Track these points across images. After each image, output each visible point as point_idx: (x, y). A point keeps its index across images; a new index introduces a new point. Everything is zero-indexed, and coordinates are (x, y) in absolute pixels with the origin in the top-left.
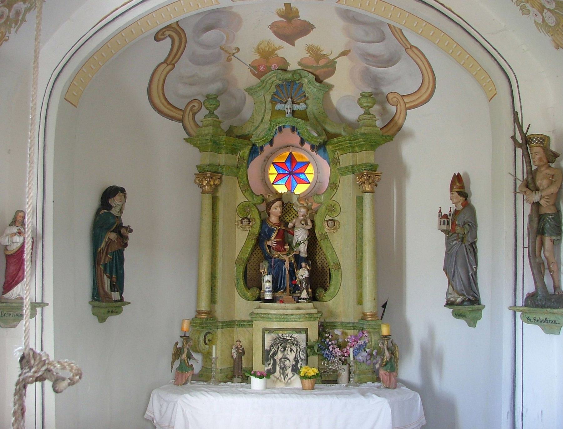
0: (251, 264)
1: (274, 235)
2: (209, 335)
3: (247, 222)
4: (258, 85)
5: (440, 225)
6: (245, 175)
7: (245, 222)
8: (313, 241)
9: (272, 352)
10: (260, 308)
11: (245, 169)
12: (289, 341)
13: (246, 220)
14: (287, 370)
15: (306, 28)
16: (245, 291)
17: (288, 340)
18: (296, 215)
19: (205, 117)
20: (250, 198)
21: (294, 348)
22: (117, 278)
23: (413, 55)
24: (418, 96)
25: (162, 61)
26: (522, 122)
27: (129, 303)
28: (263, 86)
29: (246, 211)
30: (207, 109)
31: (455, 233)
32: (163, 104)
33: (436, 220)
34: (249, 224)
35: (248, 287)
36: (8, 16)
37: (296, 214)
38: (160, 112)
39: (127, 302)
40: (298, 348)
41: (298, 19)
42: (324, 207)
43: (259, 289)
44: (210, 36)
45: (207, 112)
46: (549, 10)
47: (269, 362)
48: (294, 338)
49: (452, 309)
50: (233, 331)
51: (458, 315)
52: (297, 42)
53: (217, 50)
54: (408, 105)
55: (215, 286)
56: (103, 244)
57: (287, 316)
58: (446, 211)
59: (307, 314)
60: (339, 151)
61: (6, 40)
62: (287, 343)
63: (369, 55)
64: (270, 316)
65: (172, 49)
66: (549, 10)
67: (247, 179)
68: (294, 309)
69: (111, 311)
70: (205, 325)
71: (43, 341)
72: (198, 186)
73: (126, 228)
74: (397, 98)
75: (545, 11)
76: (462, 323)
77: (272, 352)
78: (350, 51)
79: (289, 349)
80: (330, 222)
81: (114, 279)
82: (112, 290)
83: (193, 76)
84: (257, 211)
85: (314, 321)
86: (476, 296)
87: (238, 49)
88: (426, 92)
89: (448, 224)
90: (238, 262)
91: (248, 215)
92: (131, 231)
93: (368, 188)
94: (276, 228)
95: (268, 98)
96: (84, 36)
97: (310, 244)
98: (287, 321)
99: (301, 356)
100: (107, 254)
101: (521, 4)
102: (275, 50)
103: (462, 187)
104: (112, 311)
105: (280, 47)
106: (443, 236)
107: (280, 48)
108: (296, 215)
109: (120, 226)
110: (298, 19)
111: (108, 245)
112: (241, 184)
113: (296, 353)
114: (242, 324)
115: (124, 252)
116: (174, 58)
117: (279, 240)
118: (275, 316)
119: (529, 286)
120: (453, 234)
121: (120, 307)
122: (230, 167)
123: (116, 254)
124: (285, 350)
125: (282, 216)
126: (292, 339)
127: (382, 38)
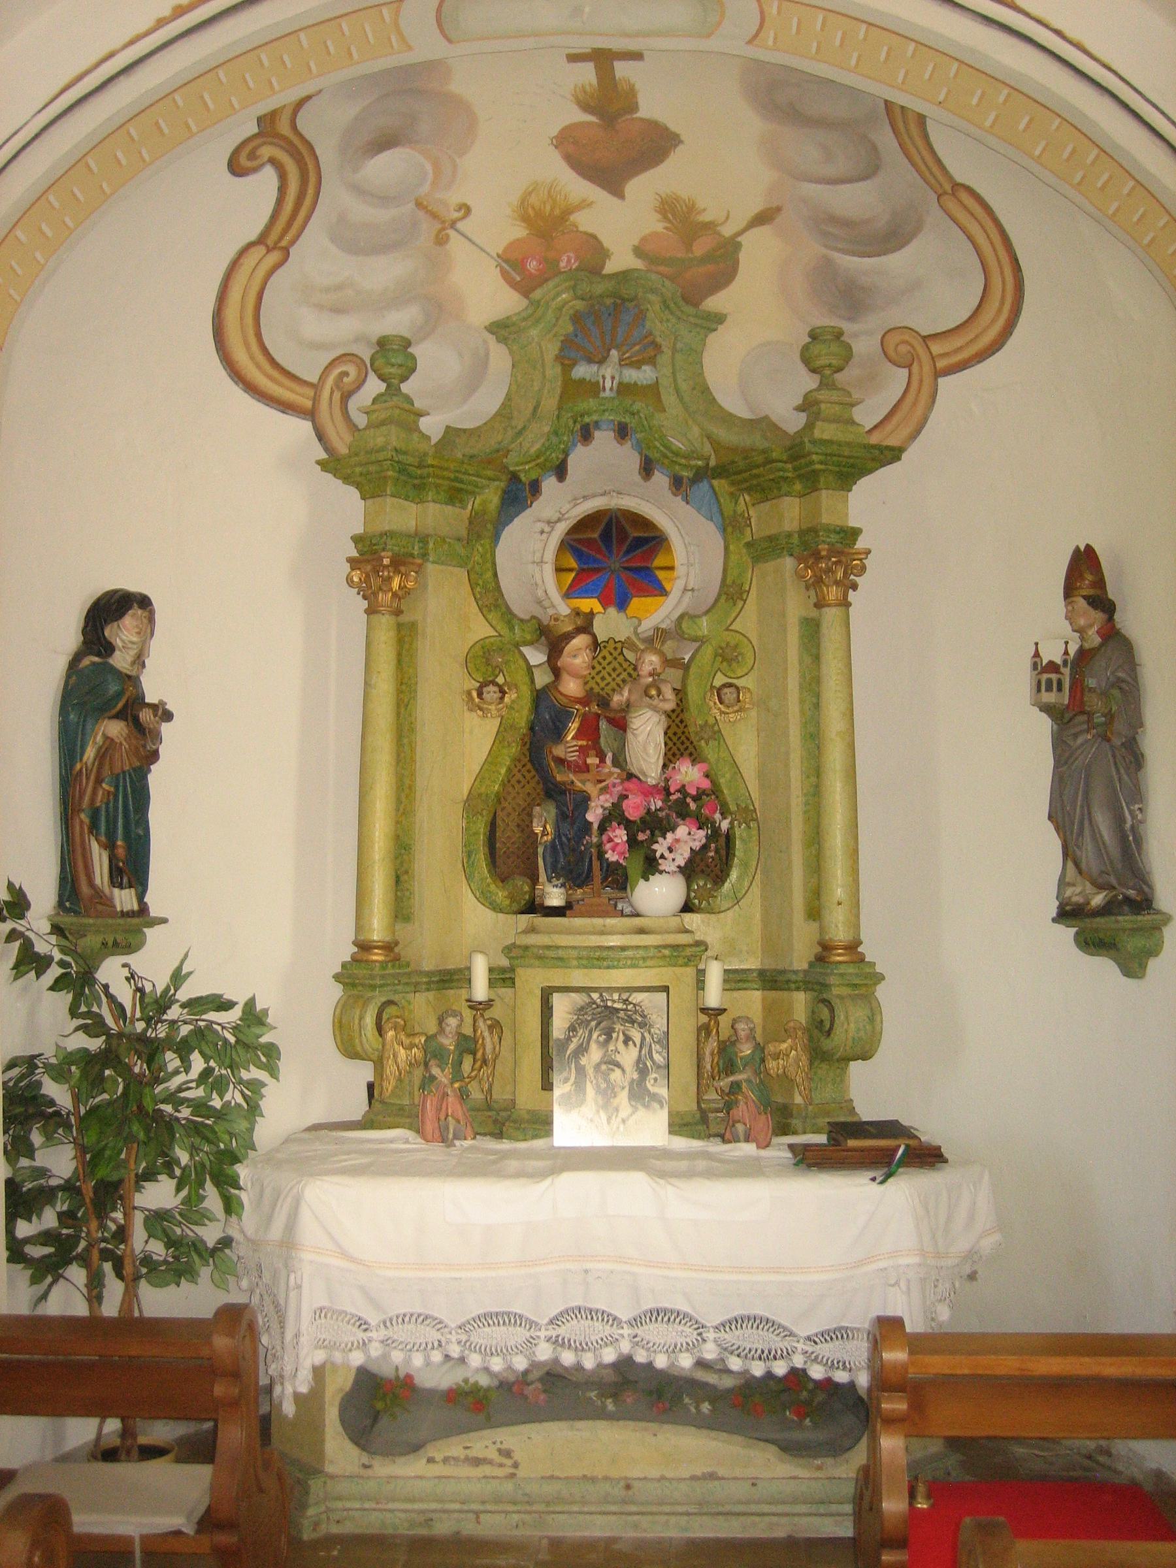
0: (505, 812)
1: (574, 727)
2: (391, 1010)
3: (495, 692)
4: (524, 314)
5: (1039, 690)
6: (489, 565)
7: (489, 692)
8: (679, 744)
9: (572, 1046)
10: (532, 930)
11: (488, 547)
12: (622, 1014)
13: (491, 688)
14: (615, 1096)
16: (493, 887)
17: (617, 1010)
18: (630, 675)
19: (375, 401)
20: (505, 631)
21: (636, 1034)
22: (129, 848)
23: (961, 216)
24: (971, 336)
25: (253, 237)
27: (164, 921)
29: (494, 664)
30: (382, 378)
31: (1082, 712)
32: (259, 367)
33: (1024, 679)
34: (502, 698)
35: (503, 879)
37: (632, 672)
38: (250, 388)
39: (160, 918)
40: (646, 1035)
41: (635, 116)
42: (708, 651)
43: (528, 880)
45: (382, 387)
47: (565, 1074)
48: (635, 1005)
49: (1075, 929)
51: (1091, 943)
54: (941, 364)
57: (610, 953)
58: (1052, 653)
59: (666, 947)
60: (749, 494)
62: (615, 1019)
63: (833, 219)
64: (561, 953)
65: (280, 201)
67: (495, 575)
68: (630, 933)
69: (110, 943)
70: (378, 982)
72: (359, 594)
73: (154, 707)
76: (1104, 967)
77: (572, 1046)
78: (779, 209)
79: (621, 1037)
80: (726, 690)
81: (121, 852)
82: (113, 883)
83: (339, 287)
84: (521, 662)
85: (686, 965)
86: (1146, 889)
87: (466, 210)
88: (993, 321)
89: (1060, 689)
90: (471, 804)
91: (497, 676)
92: (168, 716)
93: (833, 593)
94: (577, 710)
95: (552, 349)
96: (15, 133)
98: (608, 967)
99: (656, 1057)
100: (99, 781)
102: (568, 212)
103: (1100, 583)
104: (115, 940)
105: (584, 201)
106: (1044, 725)
107: (584, 205)
108: (630, 675)
109: (138, 700)
110: (635, 116)
111: (103, 755)
112: (478, 589)
113: (641, 1048)
115: (149, 776)
117: (584, 743)
118: (574, 953)
120: (1075, 715)
121: (138, 931)
122: (448, 540)
123: (124, 779)
124: (609, 1037)
125: (593, 678)
126: (630, 1007)
127: (870, 169)
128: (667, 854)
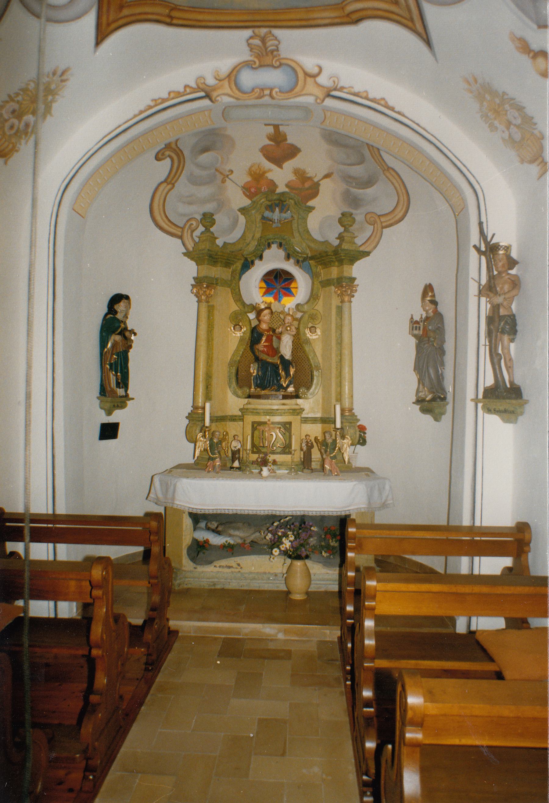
4: (250, 206)
6: (237, 287)
8: (297, 345)
13: (238, 327)
15: (293, 151)
20: (242, 309)
25: (163, 179)
26: (487, 232)
27: (133, 399)
28: (254, 206)
30: (204, 226)
33: (407, 325)
34: (241, 330)
36: (18, 128)
42: (307, 316)
44: (205, 158)
46: (515, 125)
50: (226, 425)
51: (425, 410)
52: (286, 165)
53: (213, 171)
54: (384, 224)
55: (210, 385)
56: (109, 345)
58: (417, 318)
59: (290, 409)
61: (17, 151)
63: (350, 177)
66: (515, 125)
69: (116, 405)
71: (54, 428)
74: (374, 218)
75: (512, 127)
76: (428, 418)
80: (313, 328)
81: (120, 377)
85: (297, 415)
87: (231, 172)
90: (230, 365)
92: (135, 334)
97: (294, 349)
98: (273, 415)
101: (490, 122)
102: (265, 172)
106: (413, 341)
107: (270, 170)
109: (126, 329)
114: (233, 419)
116: (173, 179)
119: (490, 381)
127: (361, 161)
128: (267, 214)
